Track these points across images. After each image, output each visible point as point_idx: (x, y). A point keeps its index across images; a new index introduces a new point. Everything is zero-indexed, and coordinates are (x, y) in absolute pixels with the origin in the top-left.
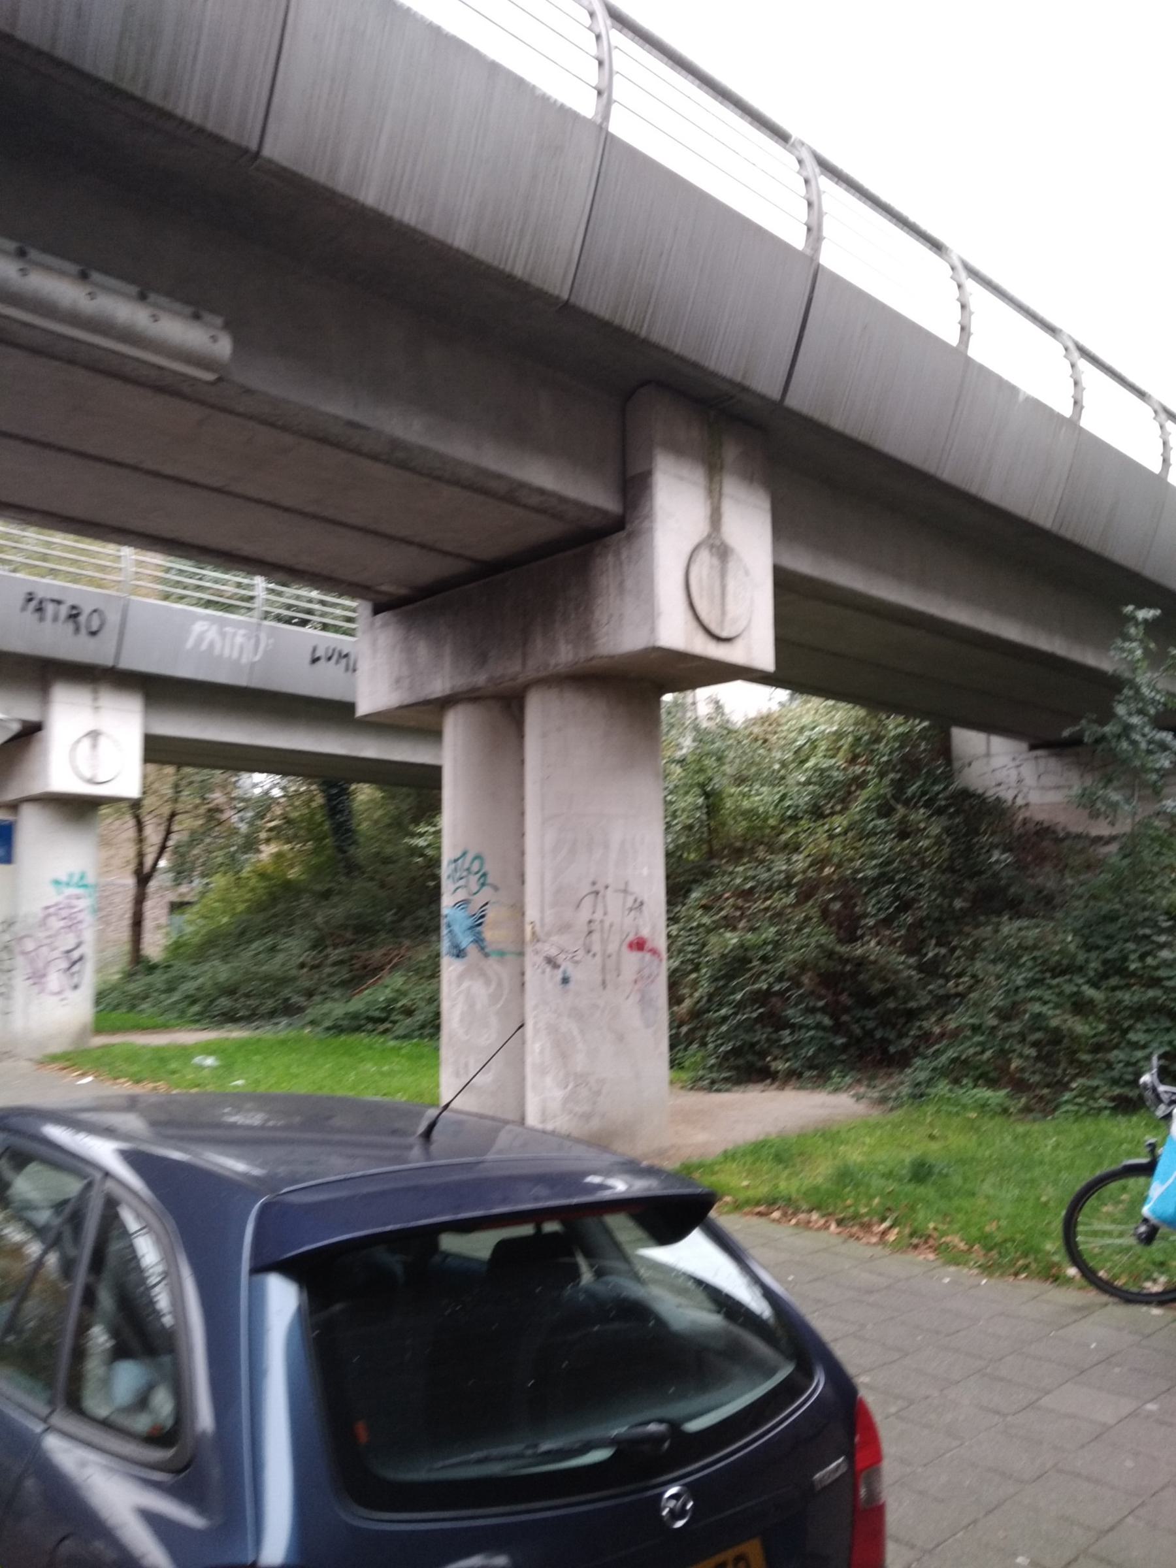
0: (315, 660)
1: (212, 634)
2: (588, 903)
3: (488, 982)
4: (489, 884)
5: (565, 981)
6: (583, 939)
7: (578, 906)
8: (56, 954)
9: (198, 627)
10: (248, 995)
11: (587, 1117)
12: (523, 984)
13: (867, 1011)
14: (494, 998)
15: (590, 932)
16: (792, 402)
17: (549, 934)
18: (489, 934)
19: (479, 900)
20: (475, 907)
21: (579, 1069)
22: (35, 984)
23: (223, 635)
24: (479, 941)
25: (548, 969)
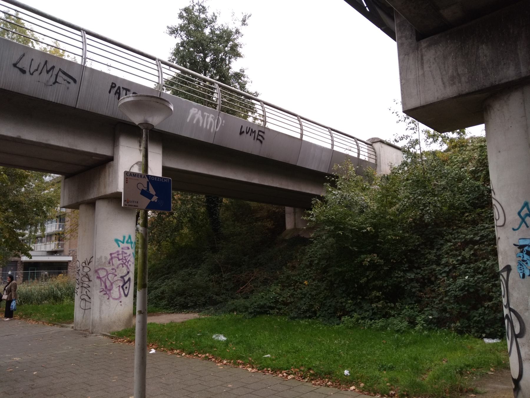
0: (241, 133)
1: (199, 115)
8: (116, 278)
9: (193, 111)
10: (191, 296)
16: (214, 143)
22: (105, 294)
23: (203, 116)
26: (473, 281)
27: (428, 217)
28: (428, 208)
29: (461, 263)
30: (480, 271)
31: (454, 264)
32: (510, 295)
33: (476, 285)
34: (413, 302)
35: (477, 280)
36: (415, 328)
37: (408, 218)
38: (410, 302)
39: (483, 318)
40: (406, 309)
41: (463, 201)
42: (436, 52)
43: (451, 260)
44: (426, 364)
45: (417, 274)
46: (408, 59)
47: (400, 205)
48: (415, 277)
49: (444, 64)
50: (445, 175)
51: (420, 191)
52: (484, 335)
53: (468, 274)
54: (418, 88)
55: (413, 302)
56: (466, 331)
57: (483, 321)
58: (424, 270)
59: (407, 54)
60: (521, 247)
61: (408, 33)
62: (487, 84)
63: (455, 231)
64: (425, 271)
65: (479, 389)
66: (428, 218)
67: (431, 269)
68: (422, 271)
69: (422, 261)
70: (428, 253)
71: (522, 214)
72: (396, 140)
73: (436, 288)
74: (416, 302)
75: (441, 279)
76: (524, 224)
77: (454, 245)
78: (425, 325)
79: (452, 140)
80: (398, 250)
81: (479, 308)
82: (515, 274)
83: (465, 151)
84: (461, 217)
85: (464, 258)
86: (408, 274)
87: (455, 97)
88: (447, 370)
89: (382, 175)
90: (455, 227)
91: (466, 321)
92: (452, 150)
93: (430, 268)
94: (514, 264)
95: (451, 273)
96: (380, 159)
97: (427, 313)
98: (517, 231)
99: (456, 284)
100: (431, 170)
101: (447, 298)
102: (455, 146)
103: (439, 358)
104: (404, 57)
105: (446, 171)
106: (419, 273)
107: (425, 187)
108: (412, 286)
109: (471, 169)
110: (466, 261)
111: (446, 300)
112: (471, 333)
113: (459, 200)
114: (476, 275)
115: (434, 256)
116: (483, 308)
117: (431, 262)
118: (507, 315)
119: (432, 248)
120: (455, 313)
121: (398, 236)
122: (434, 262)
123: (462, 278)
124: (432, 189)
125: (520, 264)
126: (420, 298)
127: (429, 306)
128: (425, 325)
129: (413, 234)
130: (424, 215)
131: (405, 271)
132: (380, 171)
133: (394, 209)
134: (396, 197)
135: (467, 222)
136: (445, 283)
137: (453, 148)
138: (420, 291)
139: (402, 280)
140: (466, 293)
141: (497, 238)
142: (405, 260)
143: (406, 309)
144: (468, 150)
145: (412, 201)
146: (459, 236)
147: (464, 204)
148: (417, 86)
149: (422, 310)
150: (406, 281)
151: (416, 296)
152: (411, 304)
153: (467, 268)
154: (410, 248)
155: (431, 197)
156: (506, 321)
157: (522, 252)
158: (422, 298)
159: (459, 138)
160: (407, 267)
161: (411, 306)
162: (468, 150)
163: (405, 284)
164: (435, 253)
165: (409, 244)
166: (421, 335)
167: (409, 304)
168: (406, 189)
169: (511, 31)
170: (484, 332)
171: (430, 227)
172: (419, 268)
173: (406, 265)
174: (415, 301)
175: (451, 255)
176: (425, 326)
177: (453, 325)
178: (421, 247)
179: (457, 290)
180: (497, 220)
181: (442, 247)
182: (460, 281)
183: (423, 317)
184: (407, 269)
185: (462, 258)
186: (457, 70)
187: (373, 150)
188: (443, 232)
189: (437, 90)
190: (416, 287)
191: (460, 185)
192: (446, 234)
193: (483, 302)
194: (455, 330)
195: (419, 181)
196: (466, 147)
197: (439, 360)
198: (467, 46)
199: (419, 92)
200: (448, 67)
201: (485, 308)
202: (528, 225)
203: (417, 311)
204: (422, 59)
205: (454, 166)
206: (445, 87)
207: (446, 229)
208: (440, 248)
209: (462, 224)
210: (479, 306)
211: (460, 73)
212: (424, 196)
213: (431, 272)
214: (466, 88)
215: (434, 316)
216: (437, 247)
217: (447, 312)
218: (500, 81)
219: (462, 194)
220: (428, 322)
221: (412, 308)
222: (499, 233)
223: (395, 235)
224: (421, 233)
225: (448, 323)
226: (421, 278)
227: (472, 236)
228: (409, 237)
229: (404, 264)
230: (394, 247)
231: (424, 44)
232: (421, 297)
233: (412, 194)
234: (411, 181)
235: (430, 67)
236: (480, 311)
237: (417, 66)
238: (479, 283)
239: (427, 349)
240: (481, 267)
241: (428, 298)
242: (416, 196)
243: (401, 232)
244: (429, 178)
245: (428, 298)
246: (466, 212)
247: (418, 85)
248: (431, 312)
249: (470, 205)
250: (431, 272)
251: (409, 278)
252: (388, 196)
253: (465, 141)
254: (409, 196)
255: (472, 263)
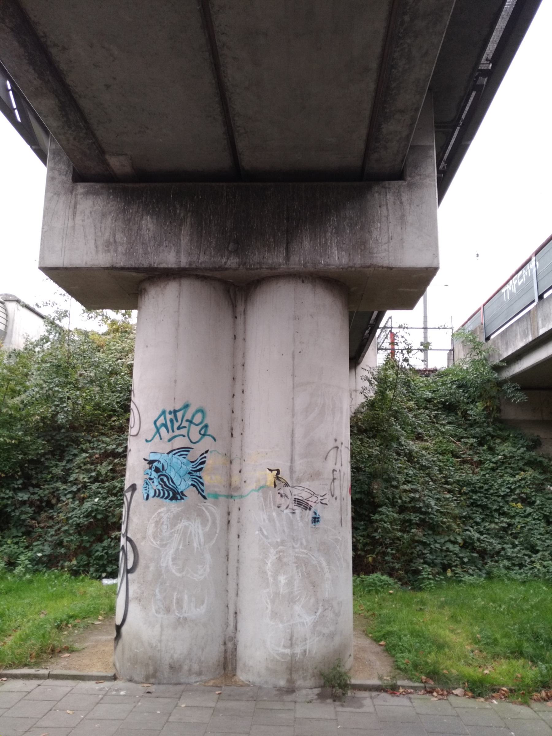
2: (332, 453)
3: (204, 523)
4: (209, 435)
5: (316, 520)
6: (329, 484)
7: (326, 458)
11: (332, 636)
12: (229, 522)
13: (424, 541)
14: (209, 537)
15: (334, 479)
17: (299, 480)
18: (206, 478)
19: (198, 449)
20: (195, 454)
21: (327, 595)
24: (198, 485)
25: (298, 510)
26: (103, 505)
27: (63, 417)
28: (65, 405)
29: (96, 480)
30: (115, 491)
31: (85, 482)
32: (130, 521)
33: (106, 510)
34: (20, 534)
35: (108, 503)
36: (14, 572)
37: (33, 415)
38: (15, 534)
39: (106, 553)
40: (7, 544)
41: (114, 401)
42: (94, 204)
43: (82, 476)
44: (16, 621)
45: (33, 494)
46: (58, 201)
47: (28, 396)
48: (29, 498)
49: (101, 223)
50: (97, 366)
51: (59, 381)
52: (104, 575)
53: (99, 495)
54: (64, 243)
55: (20, 534)
56: (83, 571)
57: (106, 556)
58: (44, 490)
59: (58, 194)
60: (151, 462)
61: (63, 168)
62: (145, 264)
63: (95, 439)
64: (44, 492)
65: (77, 646)
66: (63, 419)
67: (53, 488)
68: (41, 491)
69: (44, 476)
70: (54, 466)
71: (158, 424)
72: (37, 305)
73: (55, 514)
74: (24, 534)
75: (64, 502)
76: (158, 435)
77: (90, 457)
78: (30, 566)
79: (114, 322)
80: (11, 459)
81: (104, 540)
82: (140, 493)
83: (127, 338)
84: (107, 421)
85: (99, 474)
86: (20, 494)
87: (107, 268)
88: (42, 625)
89: (11, 350)
90: (96, 434)
91: (85, 558)
92: (112, 335)
93: (53, 486)
94: (140, 484)
95: (79, 494)
96: (13, 326)
97: (35, 549)
98: (150, 443)
99: (82, 508)
100: (79, 355)
101: (66, 528)
102: (117, 330)
103: (37, 610)
104: (53, 197)
105: (97, 359)
106: (37, 493)
107: (66, 376)
108: (22, 511)
109: (129, 363)
110: (100, 478)
111: (66, 531)
112: (88, 573)
113: (108, 399)
114: (109, 496)
115: (62, 470)
116: (109, 540)
117: (55, 478)
118: (123, 546)
119: (60, 460)
120: (73, 547)
121: (15, 439)
122: (60, 478)
123: (91, 501)
124: (76, 380)
125: (146, 483)
126: (31, 529)
127: (41, 539)
128: (30, 566)
129: (38, 437)
130: (58, 413)
131: (16, 490)
132: (10, 343)
133: (17, 400)
134: (21, 384)
135: (112, 428)
136: (68, 506)
137: (114, 332)
138: (33, 518)
139: (9, 502)
140: (92, 520)
141: (128, 450)
142: (19, 474)
143: (7, 544)
144: (130, 339)
145: (45, 392)
146: (99, 445)
147: (113, 405)
148: (63, 238)
149: (31, 544)
150: (15, 505)
151: (27, 526)
152: (17, 537)
153: (100, 488)
154: (30, 457)
155: (72, 390)
156: (121, 553)
157: (150, 468)
158: (33, 529)
159: (123, 322)
160: (21, 484)
161: (15, 540)
162: (130, 339)
163: (13, 508)
164: (64, 466)
165: (30, 452)
166: (20, 581)
167: (14, 537)
168: (40, 375)
169: (178, 212)
170: (105, 571)
171: (63, 431)
172: (38, 486)
173: (20, 482)
174: (22, 533)
175: (83, 470)
176: (29, 568)
177: (67, 564)
178: (47, 456)
179: (81, 516)
180: (131, 428)
181: (75, 458)
182: (87, 505)
183: (29, 554)
184: (20, 486)
185: (97, 475)
186: (114, 236)
187: (4, 311)
188: (79, 439)
189: (87, 253)
190: (28, 513)
191: (113, 379)
192: (84, 442)
193: (110, 532)
194: (69, 570)
195: (60, 366)
196: (129, 334)
197: (36, 613)
198: (131, 211)
199: (63, 249)
200: (105, 229)
201: (112, 539)
202: (162, 437)
203: (22, 547)
204: (75, 207)
205: (111, 354)
206: (97, 252)
207: (85, 435)
208: (72, 460)
209: (106, 430)
210: (106, 537)
211: (117, 240)
212: (62, 387)
213: (54, 492)
214: (121, 261)
215: (44, 553)
216: (67, 458)
217: (63, 547)
218: (159, 264)
219: (113, 392)
220: (35, 562)
221: (17, 543)
222: (132, 444)
223: (11, 438)
224: (50, 438)
225: (61, 562)
226: (38, 500)
227: (114, 446)
228: (31, 441)
229: (18, 480)
230: (6, 455)
231: (81, 188)
232: (31, 527)
233: (47, 382)
234: (48, 365)
235: (83, 221)
236: (105, 543)
237: (67, 214)
238: (110, 507)
239: (24, 599)
240: (117, 487)
241: (42, 528)
242: (51, 386)
243: (20, 433)
244: (74, 364)
245: (42, 528)
246: (115, 415)
247: (64, 239)
248: (41, 547)
249: (120, 407)
250: (54, 492)
251: (20, 499)
252: (11, 380)
253: (129, 326)
254: (41, 385)
255: (107, 481)
